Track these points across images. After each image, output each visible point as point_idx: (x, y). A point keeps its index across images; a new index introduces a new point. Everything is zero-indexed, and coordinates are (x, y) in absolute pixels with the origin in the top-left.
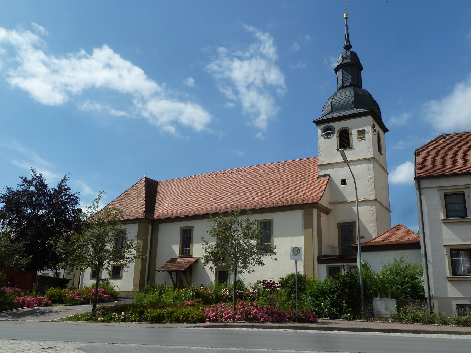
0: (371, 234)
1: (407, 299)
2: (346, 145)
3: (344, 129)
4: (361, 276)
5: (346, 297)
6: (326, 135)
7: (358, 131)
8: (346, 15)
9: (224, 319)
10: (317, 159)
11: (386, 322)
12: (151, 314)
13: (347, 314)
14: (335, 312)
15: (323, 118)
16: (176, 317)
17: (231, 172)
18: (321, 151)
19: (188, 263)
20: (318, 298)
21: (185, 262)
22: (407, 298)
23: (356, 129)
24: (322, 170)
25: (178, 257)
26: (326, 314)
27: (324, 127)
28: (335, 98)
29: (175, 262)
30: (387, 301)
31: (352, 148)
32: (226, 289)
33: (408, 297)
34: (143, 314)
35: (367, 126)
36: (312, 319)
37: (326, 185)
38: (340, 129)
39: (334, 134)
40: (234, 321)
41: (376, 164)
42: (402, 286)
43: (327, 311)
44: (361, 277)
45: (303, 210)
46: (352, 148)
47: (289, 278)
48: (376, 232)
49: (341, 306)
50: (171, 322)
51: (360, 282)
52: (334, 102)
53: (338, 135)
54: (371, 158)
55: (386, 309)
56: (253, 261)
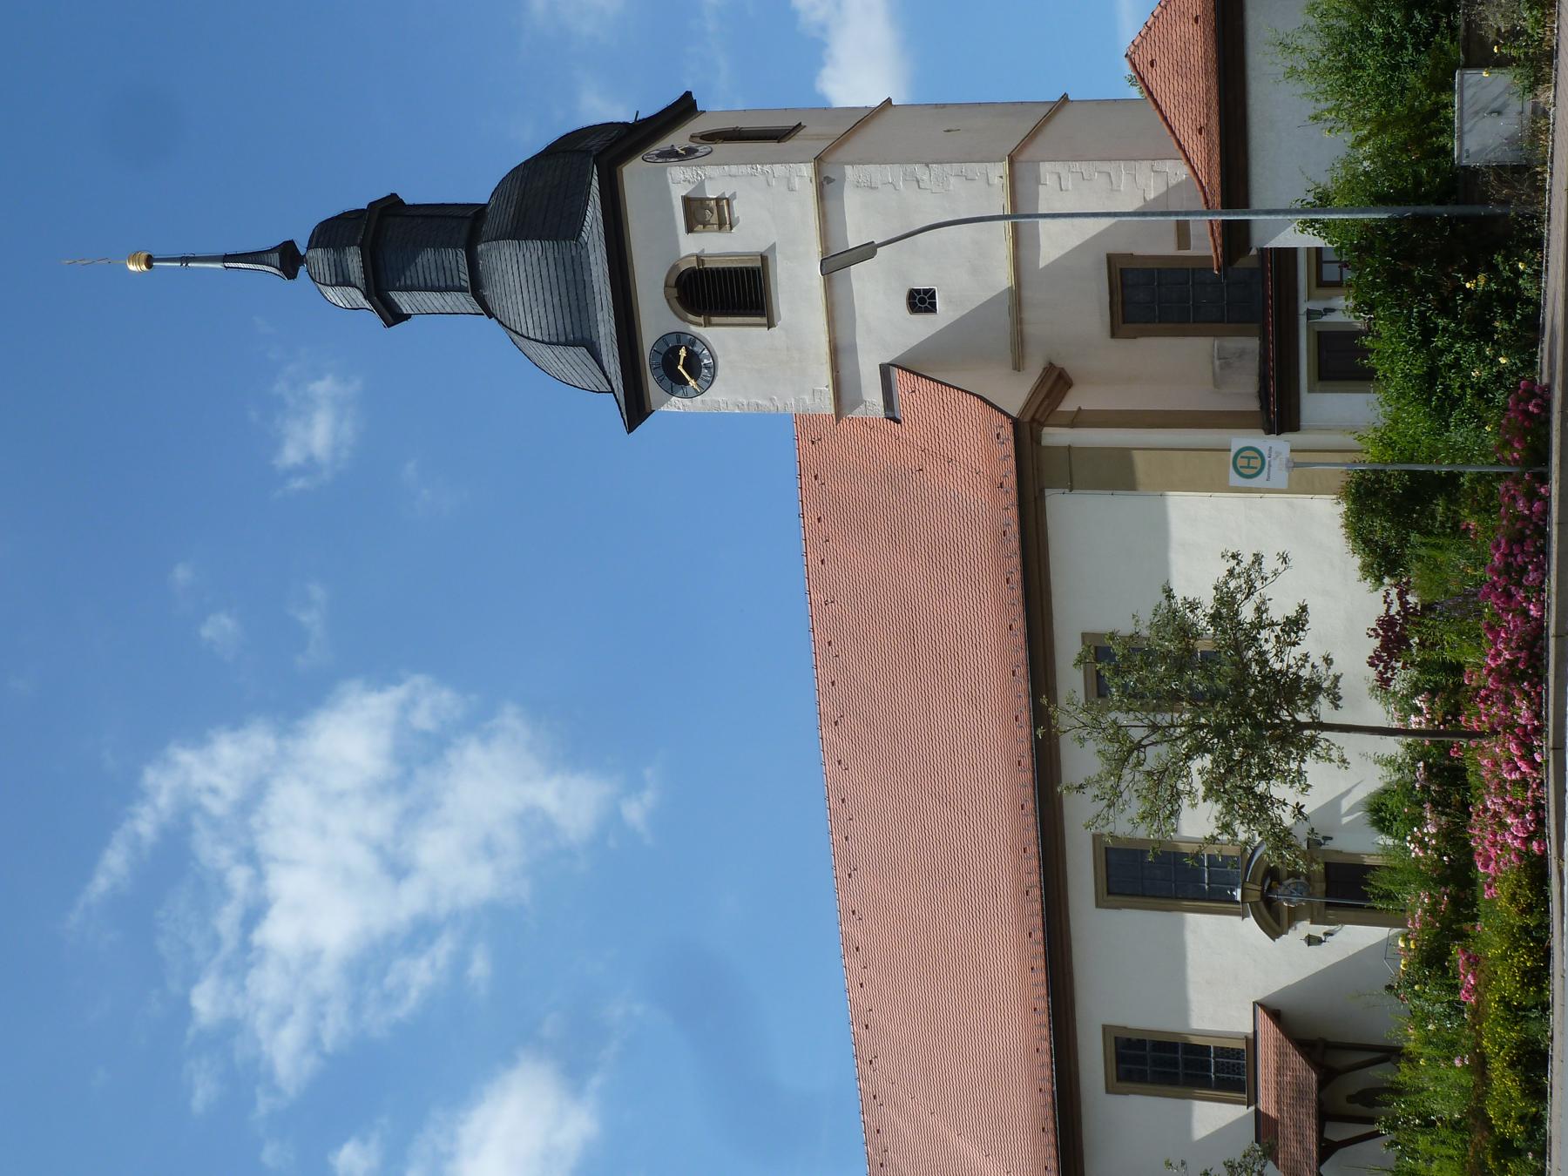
0: (1165, 189)
1: (1458, 28)
2: (750, 288)
3: (674, 292)
4: (1358, 213)
5: (1448, 276)
6: (695, 374)
7: (690, 229)
8: (134, 258)
9: (1535, 775)
10: (804, 422)
11: (1551, 112)
12: (1511, 1099)
13: (1519, 274)
14: (1510, 323)
15: (618, 384)
16: (1522, 987)
17: (847, 838)
18: (771, 399)
19: (1281, 1054)
20: (1449, 397)
21: (1280, 1071)
22: (1452, 28)
23: (676, 236)
24: (859, 401)
25: (1252, 1108)
26: (1519, 364)
27: (659, 382)
28: (524, 327)
29: (1275, 1122)
30: (1466, 107)
31: (764, 258)
32: (1409, 838)
33: (1449, 23)
34: (1510, 1141)
35: (668, 187)
36: (1536, 405)
37: (934, 380)
38: (676, 313)
39: (694, 340)
40: (1539, 731)
41: (840, 154)
42: (1402, 46)
43: (1507, 356)
44: (1363, 212)
45: (1048, 492)
46: (764, 258)
47: (1366, 542)
48: (1158, 165)
49: (1485, 301)
50: (1546, 1007)
51: (1385, 216)
52: (545, 332)
53: (701, 320)
54: (818, 172)
55: (1499, 113)
56: (1286, 658)
